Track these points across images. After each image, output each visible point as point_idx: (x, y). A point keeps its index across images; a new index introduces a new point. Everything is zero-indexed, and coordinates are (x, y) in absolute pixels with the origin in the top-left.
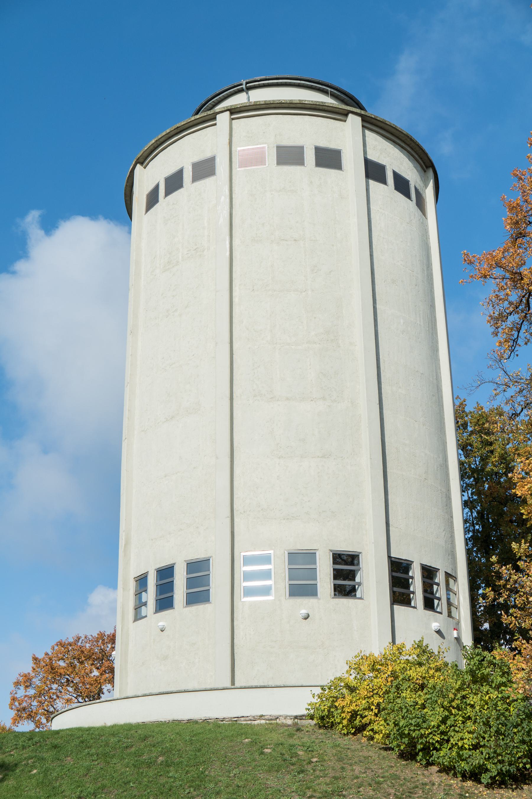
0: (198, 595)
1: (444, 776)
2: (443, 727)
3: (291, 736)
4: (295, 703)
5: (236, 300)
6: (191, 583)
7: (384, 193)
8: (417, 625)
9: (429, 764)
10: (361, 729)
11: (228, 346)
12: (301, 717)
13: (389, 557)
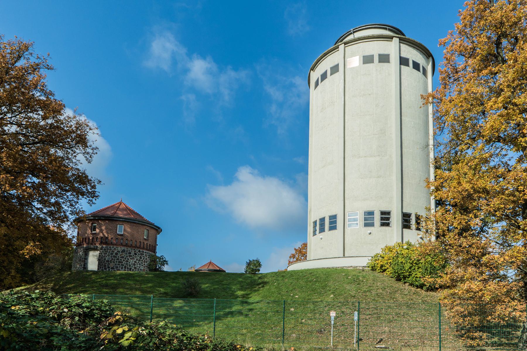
0: (333, 227)
1: (410, 286)
2: (410, 270)
3: (360, 273)
4: (363, 262)
5: (346, 121)
6: (331, 223)
7: (408, 70)
8: (413, 236)
9: (405, 283)
10: (385, 270)
11: (343, 139)
12: (365, 267)
13: (402, 212)
